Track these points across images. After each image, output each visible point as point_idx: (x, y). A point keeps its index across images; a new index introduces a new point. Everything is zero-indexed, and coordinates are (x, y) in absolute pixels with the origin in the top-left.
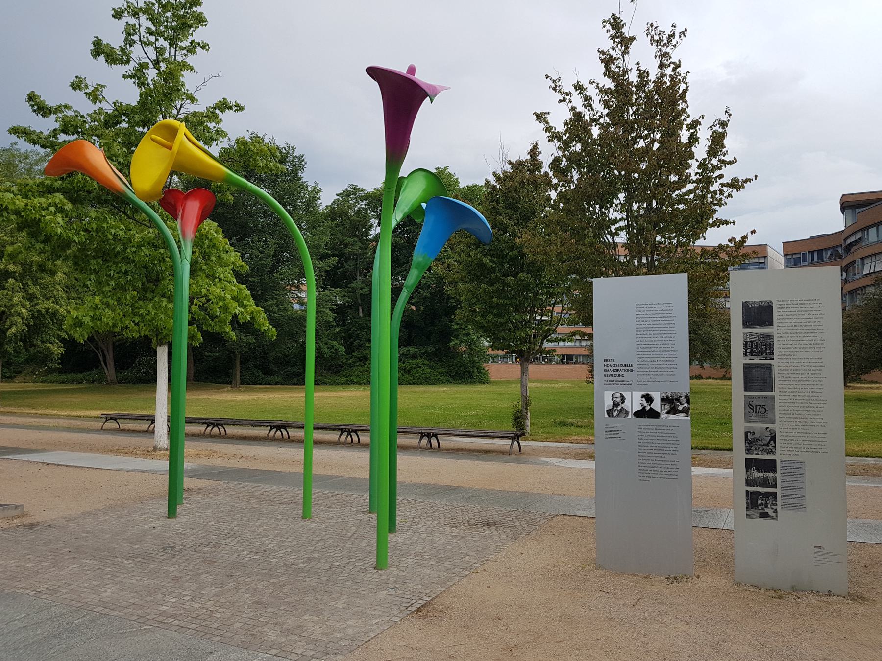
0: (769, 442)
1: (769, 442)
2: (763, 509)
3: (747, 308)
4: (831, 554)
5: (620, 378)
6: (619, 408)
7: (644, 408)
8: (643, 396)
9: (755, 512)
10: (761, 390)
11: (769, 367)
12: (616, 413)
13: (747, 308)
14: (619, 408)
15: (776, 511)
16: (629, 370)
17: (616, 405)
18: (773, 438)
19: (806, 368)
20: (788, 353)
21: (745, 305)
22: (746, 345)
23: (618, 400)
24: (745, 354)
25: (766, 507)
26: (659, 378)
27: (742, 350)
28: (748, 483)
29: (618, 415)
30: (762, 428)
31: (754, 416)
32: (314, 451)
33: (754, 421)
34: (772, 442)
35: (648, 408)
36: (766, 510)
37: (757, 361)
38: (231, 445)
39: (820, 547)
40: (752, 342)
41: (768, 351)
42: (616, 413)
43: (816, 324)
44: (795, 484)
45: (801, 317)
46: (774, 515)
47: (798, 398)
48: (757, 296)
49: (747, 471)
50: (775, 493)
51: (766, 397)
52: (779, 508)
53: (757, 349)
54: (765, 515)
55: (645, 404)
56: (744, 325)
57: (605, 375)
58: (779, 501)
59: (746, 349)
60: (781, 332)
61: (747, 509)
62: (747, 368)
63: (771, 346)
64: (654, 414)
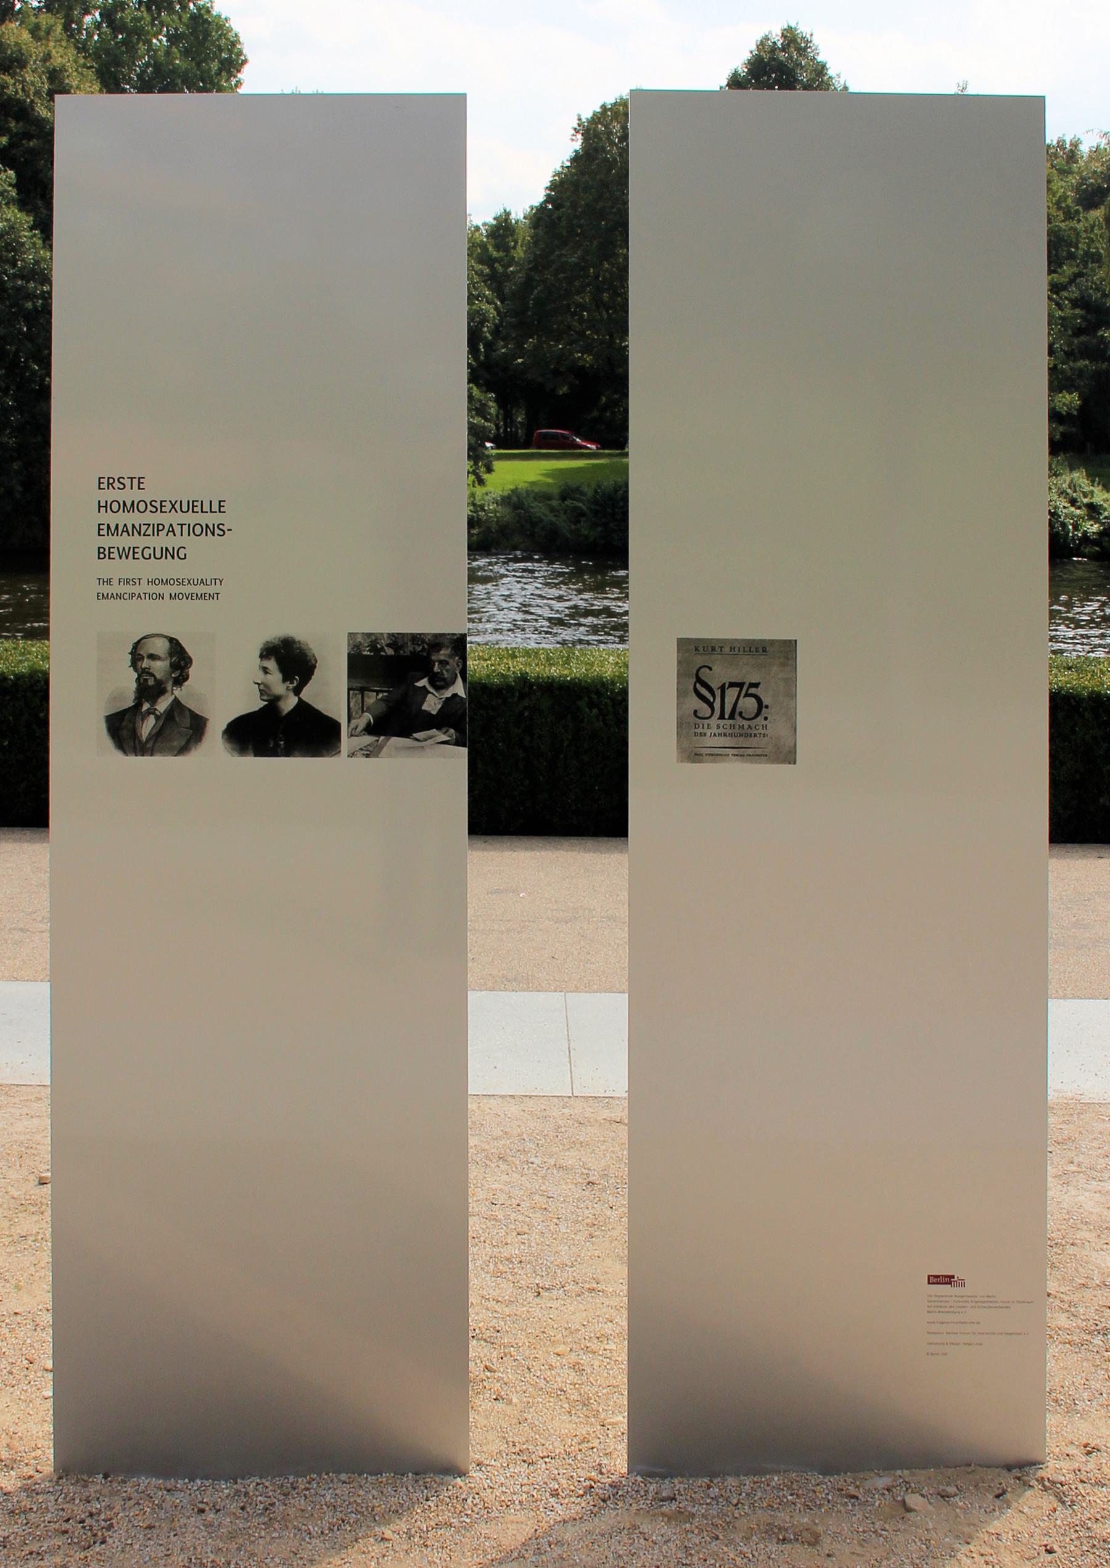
6: (163, 705)
7: (273, 702)
8: (270, 651)
12: (147, 727)
14: (163, 705)
16: (209, 530)
17: (148, 690)
23: (159, 668)
29: (158, 735)
32: (469, 857)
35: (289, 704)
38: (507, 854)
39: (948, 1280)
42: (147, 727)
55: (276, 682)
64: (309, 733)
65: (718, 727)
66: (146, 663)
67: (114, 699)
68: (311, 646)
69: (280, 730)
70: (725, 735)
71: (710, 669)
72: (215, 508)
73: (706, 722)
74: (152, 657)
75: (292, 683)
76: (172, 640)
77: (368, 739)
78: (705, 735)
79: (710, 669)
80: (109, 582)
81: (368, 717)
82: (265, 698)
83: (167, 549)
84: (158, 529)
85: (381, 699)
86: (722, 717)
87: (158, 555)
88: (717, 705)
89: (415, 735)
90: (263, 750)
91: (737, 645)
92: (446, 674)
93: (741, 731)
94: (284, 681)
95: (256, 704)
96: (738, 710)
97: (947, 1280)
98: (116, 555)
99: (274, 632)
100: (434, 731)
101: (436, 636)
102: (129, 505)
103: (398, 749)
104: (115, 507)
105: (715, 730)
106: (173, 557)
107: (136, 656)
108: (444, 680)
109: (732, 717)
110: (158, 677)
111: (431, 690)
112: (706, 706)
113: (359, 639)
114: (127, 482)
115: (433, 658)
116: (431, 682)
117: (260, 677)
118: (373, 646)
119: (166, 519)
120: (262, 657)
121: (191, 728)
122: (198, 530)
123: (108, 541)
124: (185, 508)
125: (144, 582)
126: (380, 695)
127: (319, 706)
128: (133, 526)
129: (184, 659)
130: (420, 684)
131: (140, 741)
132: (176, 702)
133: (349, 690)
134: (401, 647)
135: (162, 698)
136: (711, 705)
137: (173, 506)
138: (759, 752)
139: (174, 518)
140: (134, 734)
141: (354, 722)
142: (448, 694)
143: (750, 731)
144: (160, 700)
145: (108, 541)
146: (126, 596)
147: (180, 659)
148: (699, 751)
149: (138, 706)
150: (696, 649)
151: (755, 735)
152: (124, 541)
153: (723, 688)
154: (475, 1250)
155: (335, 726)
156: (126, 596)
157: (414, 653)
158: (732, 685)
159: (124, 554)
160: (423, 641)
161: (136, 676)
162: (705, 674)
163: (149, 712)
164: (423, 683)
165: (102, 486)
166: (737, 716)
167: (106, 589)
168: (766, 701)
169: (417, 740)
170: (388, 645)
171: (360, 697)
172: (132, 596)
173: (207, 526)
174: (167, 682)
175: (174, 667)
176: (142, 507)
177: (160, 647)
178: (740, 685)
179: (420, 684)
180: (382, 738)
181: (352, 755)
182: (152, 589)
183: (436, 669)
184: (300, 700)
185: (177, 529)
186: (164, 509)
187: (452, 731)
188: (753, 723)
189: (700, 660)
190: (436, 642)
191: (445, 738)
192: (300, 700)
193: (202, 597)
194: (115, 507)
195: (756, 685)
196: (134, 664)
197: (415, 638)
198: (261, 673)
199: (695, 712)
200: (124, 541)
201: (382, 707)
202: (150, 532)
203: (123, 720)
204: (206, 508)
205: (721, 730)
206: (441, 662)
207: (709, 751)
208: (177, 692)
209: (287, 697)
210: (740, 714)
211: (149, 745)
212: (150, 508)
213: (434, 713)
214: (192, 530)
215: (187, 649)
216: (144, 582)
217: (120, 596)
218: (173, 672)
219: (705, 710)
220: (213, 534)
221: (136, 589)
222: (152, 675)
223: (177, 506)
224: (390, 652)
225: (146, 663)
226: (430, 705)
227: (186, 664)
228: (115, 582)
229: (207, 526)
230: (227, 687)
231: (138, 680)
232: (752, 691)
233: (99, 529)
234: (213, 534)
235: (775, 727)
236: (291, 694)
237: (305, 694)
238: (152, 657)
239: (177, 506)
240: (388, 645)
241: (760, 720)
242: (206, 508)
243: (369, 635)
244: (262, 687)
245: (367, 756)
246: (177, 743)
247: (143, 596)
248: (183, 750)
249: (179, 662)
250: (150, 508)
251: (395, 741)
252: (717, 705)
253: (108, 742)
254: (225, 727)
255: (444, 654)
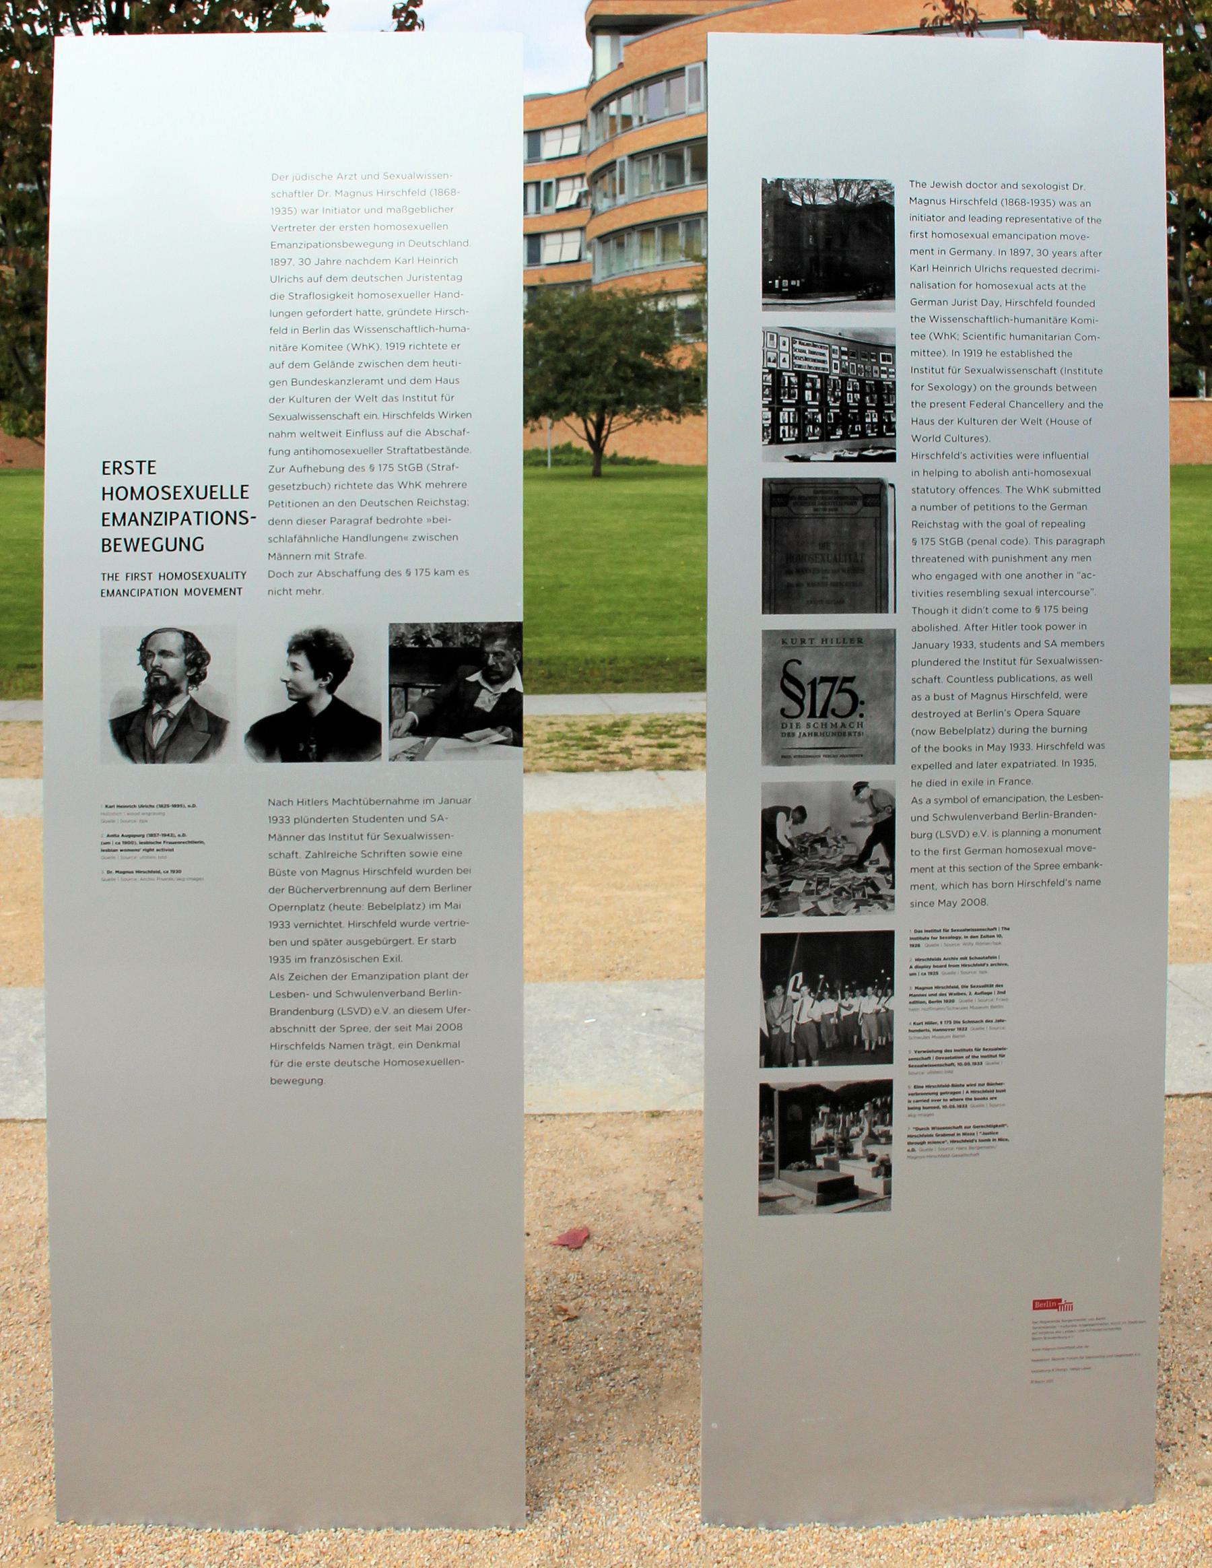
0: (866, 853)
1: (866, 853)
2: (832, 1165)
3: (782, 210)
4: (1099, 1325)
5: (183, 561)
6: (177, 706)
7: (303, 701)
8: (299, 645)
9: (796, 1185)
10: (838, 606)
11: (874, 497)
12: (158, 732)
13: (782, 210)
14: (177, 706)
15: (885, 1169)
17: (160, 691)
18: (884, 833)
19: (1027, 499)
20: (955, 430)
21: (777, 200)
22: (776, 388)
23: (173, 666)
24: (773, 435)
25: (846, 1151)
26: (378, 556)
27: (759, 415)
28: (773, 1051)
29: (170, 739)
30: (836, 786)
31: (804, 730)
32: (526, 788)
33: (805, 757)
34: (879, 850)
35: (323, 702)
36: (847, 1168)
37: (824, 465)
39: (1055, 1304)
40: (802, 376)
41: (872, 417)
42: (158, 732)
43: (1069, 295)
44: (973, 1039)
45: (1009, 261)
46: (875, 1185)
47: (992, 636)
48: (825, 162)
49: (768, 993)
50: (884, 1088)
51: (854, 639)
52: (897, 1152)
53: (824, 407)
54: (838, 1192)
56: (768, 290)
57: (108, 545)
58: (902, 1121)
59: (775, 407)
60: (928, 328)
61: (766, 1172)
62: (780, 499)
63: (883, 394)
64: (348, 735)
65: (808, 725)
66: (157, 661)
67: (120, 701)
68: (347, 638)
69: (310, 732)
70: (816, 734)
71: (800, 663)
72: (237, 493)
73: (794, 721)
74: (164, 653)
75: (325, 680)
76: (186, 635)
77: (414, 740)
78: (794, 735)
79: (800, 663)
80: (115, 577)
81: (413, 715)
82: (294, 697)
83: (181, 540)
84: (171, 518)
85: (428, 696)
86: (812, 715)
87: (171, 547)
88: (807, 702)
89: (466, 735)
90: (291, 755)
91: (829, 636)
92: (502, 668)
93: (833, 730)
94: (316, 677)
95: (283, 704)
96: (831, 706)
97: (1054, 1304)
98: (122, 547)
99: (305, 624)
100: (488, 731)
101: (490, 625)
102: (137, 491)
103: (448, 751)
104: (122, 493)
105: (804, 730)
106: (188, 548)
107: (145, 652)
108: (500, 673)
109: (824, 715)
110: (171, 675)
111: (486, 685)
112: (794, 704)
113: (403, 630)
114: (136, 466)
115: (487, 649)
116: (486, 677)
117: (288, 674)
118: (418, 638)
119: (181, 506)
120: (290, 651)
121: (209, 732)
122: (217, 518)
123: (113, 532)
124: (202, 495)
125: (155, 577)
126: (427, 692)
127: (357, 705)
128: (143, 515)
129: (201, 655)
130: (472, 679)
131: (150, 747)
132: (192, 702)
133: (391, 686)
134: (450, 639)
135: (175, 699)
136: (800, 703)
137: (189, 492)
138: (853, 752)
139: (191, 505)
140: (144, 738)
141: (396, 723)
142: (504, 688)
143: (843, 730)
144: (173, 701)
145: (113, 532)
146: (134, 593)
147: (196, 655)
148: (786, 753)
149: (148, 707)
150: (783, 642)
151: (850, 734)
152: (132, 532)
153: (813, 684)
154: (531, 1162)
155: (375, 726)
156: (134, 593)
157: (465, 645)
158: (824, 680)
159: (132, 545)
160: (476, 632)
161: (145, 674)
162: (794, 669)
163: (160, 715)
164: (476, 677)
165: (107, 471)
166: (829, 713)
167: (111, 585)
168: (862, 696)
169: (469, 740)
170: (436, 637)
171: (403, 694)
172: (141, 592)
173: (227, 514)
174: (181, 681)
175: (190, 664)
176: (153, 493)
177: (174, 642)
178: (833, 680)
179: (472, 679)
180: (429, 739)
181: (394, 758)
182: (164, 584)
183: (491, 661)
184: (334, 698)
185: (193, 518)
186: (178, 496)
187: (509, 730)
188: (847, 721)
189: (787, 654)
190: (492, 631)
191: (501, 737)
192: (334, 698)
193: (222, 592)
194: (122, 493)
195: (851, 680)
196: (143, 662)
197: (467, 628)
198: (289, 670)
199: (783, 711)
200: (132, 532)
201: (428, 707)
202: (162, 520)
203: (131, 723)
204: (227, 493)
205: (811, 730)
206: (496, 654)
207: (798, 752)
208: (193, 692)
209: (319, 695)
210: (833, 711)
211: (161, 752)
212: (161, 494)
213: (488, 710)
214: (210, 518)
215: (205, 645)
216: (155, 577)
217: (126, 593)
218: (188, 670)
219: (794, 708)
220: (235, 522)
221: (146, 585)
222: (164, 674)
223: (193, 492)
224: (438, 644)
225: (157, 661)
226: (484, 702)
227: (203, 661)
228: (122, 577)
229: (227, 514)
230: (251, 682)
231: (148, 679)
232: (847, 685)
233: (104, 519)
234: (235, 522)
235: (870, 723)
236: (324, 692)
237: (341, 692)
238: (164, 653)
239: (193, 492)
240: (436, 637)
241: (855, 718)
242: (227, 493)
243: (414, 626)
244: (290, 685)
245: (412, 759)
246: (193, 749)
247: (154, 592)
248: (200, 756)
249: (195, 659)
250: (161, 494)
251: (443, 742)
252: (807, 702)
253: (114, 749)
254: (247, 730)
255: (499, 645)
